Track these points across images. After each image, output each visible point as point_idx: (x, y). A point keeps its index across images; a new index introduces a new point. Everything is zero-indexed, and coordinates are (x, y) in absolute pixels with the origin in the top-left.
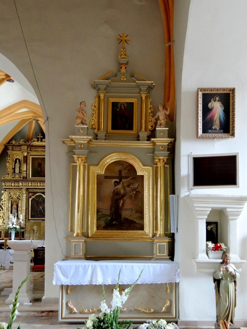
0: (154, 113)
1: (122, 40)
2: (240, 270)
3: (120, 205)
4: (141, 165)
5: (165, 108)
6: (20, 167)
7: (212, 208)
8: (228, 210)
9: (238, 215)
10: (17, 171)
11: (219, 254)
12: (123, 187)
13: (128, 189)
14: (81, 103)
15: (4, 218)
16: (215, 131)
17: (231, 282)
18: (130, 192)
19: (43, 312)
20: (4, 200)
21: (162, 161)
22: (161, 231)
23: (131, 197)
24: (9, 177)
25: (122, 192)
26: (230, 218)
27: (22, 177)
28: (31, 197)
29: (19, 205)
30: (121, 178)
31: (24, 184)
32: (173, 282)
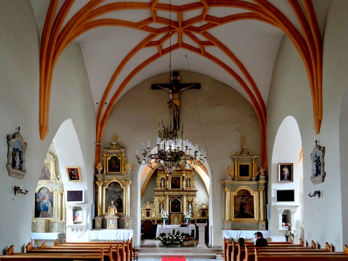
0: (258, 170)
1: (243, 138)
2: (296, 233)
3: (244, 208)
4: (253, 191)
5: (263, 168)
6: (164, 183)
7: (285, 210)
8: (291, 210)
9: (295, 212)
10: (163, 185)
11: (287, 227)
12: (245, 200)
13: (247, 201)
14: (228, 167)
15: (156, 212)
16: (285, 180)
17: (292, 237)
18: (248, 202)
19: (215, 250)
20: (155, 202)
21: (262, 190)
22: (262, 218)
23: (248, 205)
24: (159, 188)
25: (245, 202)
26: (292, 213)
27: (165, 188)
28: (171, 200)
29: (164, 205)
30: (244, 196)
31: (167, 193)
32: (269, 238)
